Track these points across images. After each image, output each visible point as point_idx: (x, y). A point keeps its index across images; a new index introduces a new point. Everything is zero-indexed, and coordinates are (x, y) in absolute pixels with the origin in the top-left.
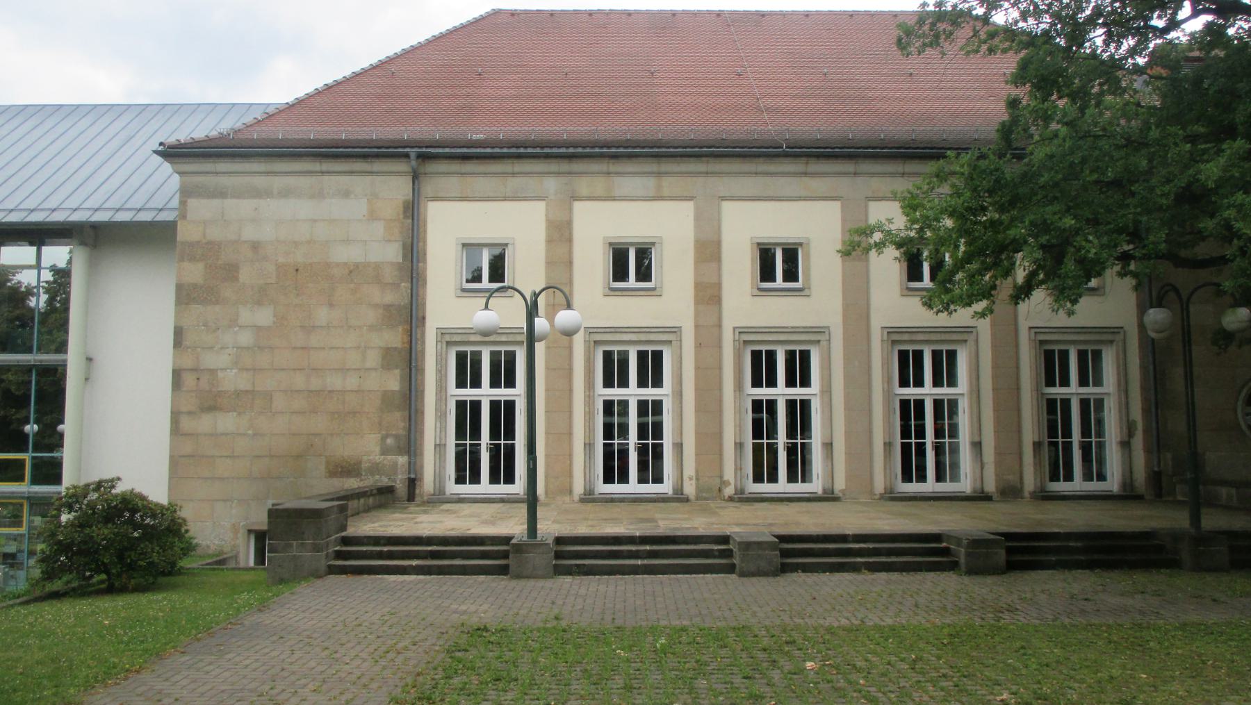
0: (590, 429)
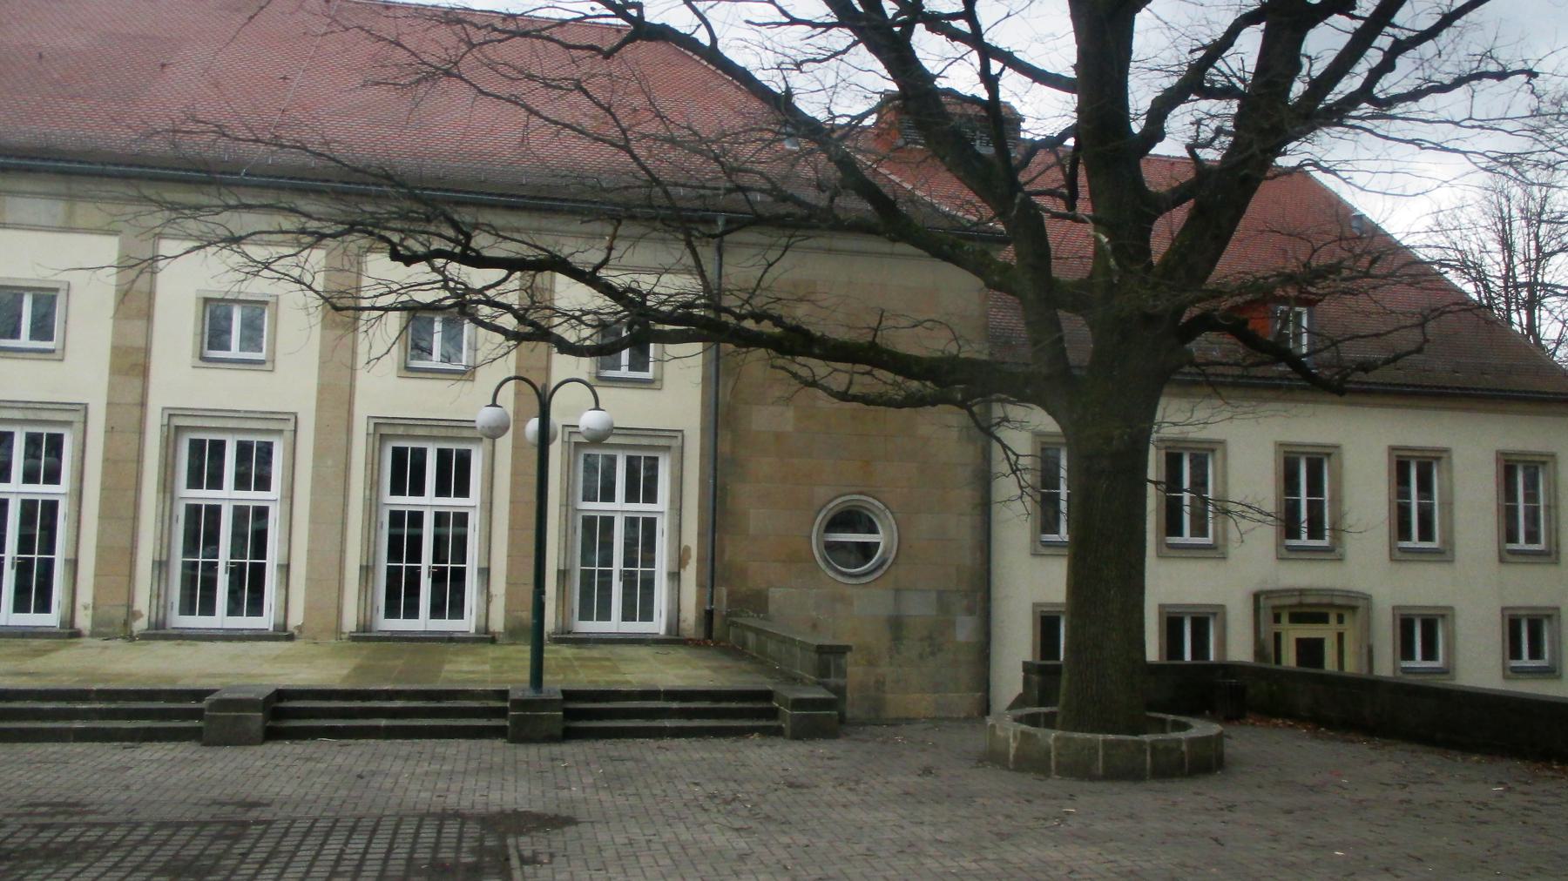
0: (165, 541)
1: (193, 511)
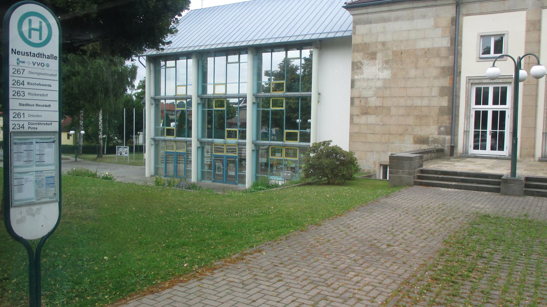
1: (477, 113)
